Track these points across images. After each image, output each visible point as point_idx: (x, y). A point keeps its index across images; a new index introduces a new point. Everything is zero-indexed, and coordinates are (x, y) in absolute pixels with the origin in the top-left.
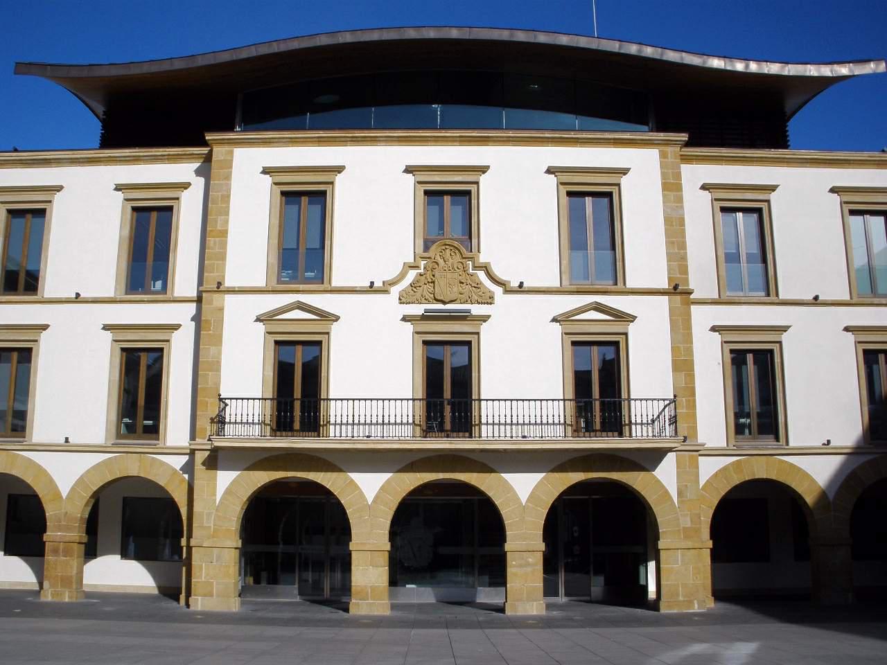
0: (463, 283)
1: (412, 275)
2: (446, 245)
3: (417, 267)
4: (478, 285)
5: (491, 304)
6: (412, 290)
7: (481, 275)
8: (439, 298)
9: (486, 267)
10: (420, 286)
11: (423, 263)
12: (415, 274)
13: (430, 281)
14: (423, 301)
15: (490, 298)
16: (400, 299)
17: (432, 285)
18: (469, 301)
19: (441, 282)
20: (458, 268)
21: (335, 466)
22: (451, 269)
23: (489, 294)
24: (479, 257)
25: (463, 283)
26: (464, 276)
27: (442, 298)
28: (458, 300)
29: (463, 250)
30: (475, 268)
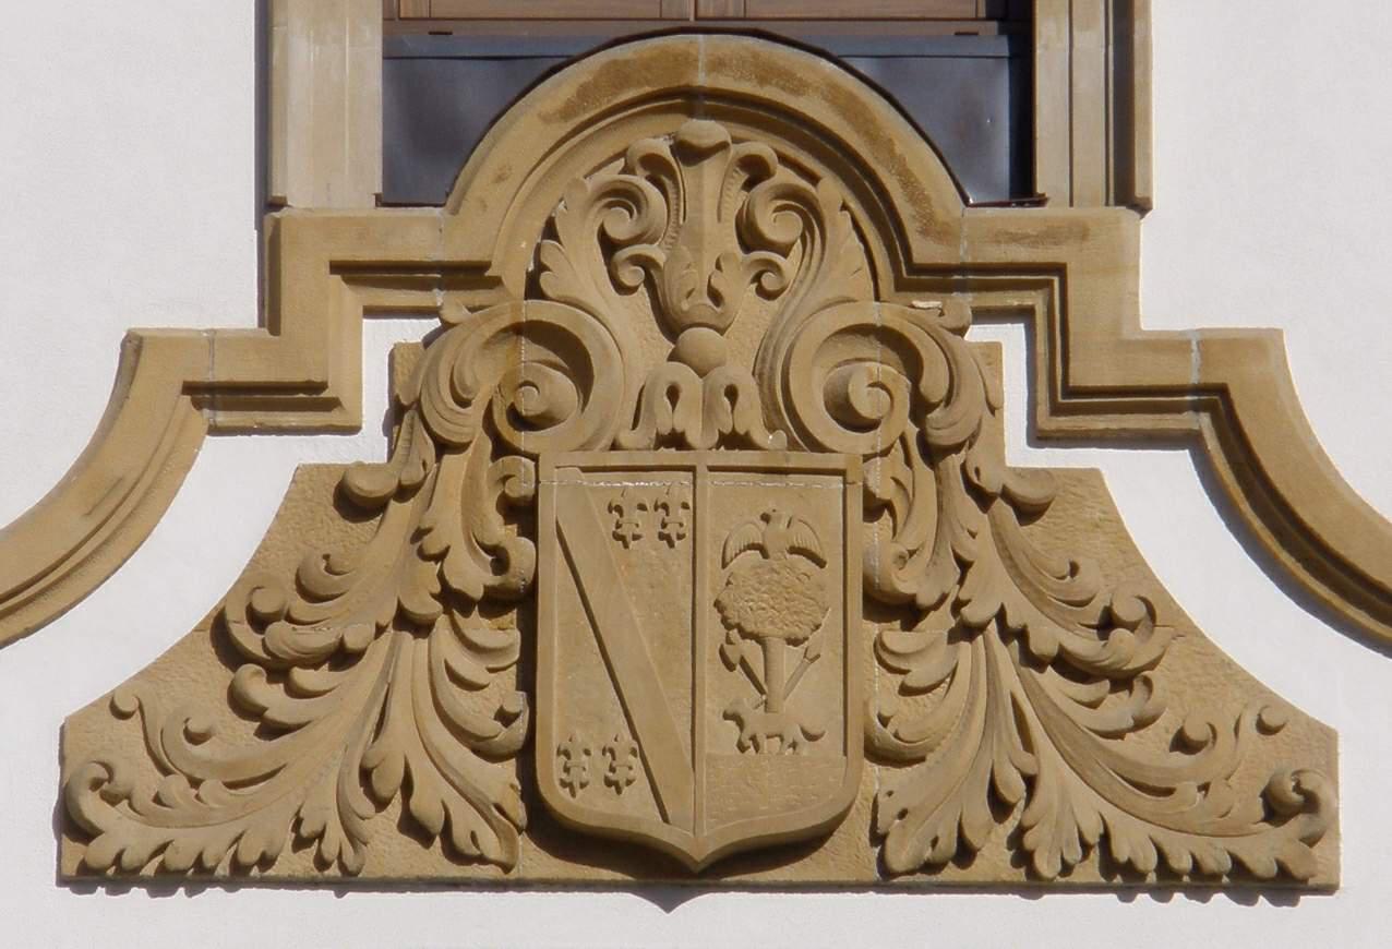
0: (909, 612)
1: (230, 505)
2: (690, 100)
3: (301, 400)
4: (1112, 646)
5: (1286, 885)
6: (241, 705)
7: (1160, 506)
8: (589, 806)
9: (1216, 399)
10: (342, 657)
11: (375, 349)
12: (280, 484)
13: (473, 576)
14: (388, 846)
15: (1275, 810)
16: (72, 825)
17: (502, 634)
18: (994, 856)
19: (622, 602)
20: (847, 416)
21: (864, 491)
22: (749, 417)
23: (1248, 766)
24: (1120, 265)
25: (909, 612)
26: (921, 527)
27: (632, 811)
28: (850, 850)
29: (915, 166)
30: (1073, 406)
